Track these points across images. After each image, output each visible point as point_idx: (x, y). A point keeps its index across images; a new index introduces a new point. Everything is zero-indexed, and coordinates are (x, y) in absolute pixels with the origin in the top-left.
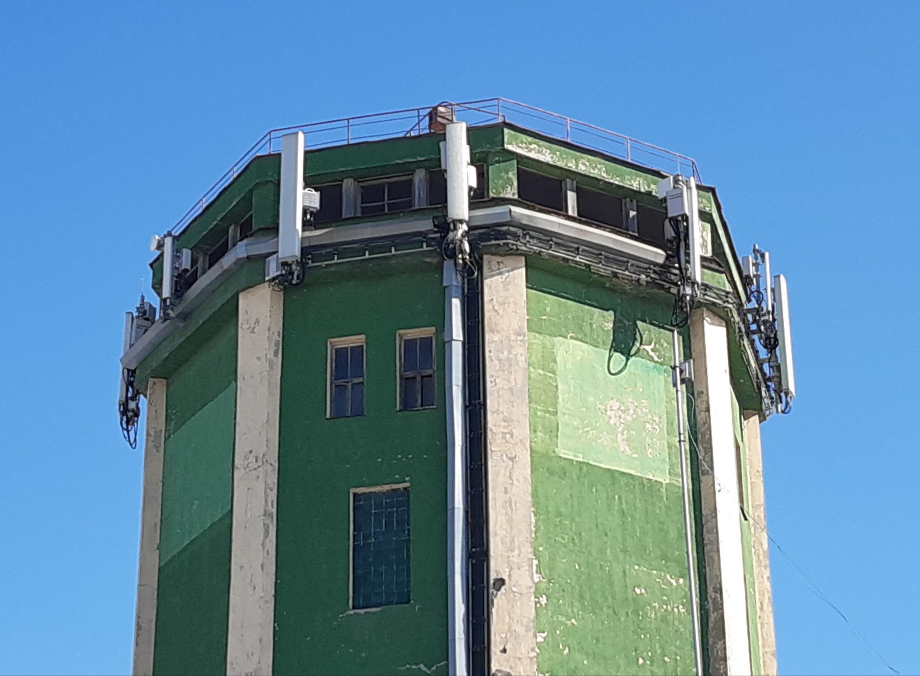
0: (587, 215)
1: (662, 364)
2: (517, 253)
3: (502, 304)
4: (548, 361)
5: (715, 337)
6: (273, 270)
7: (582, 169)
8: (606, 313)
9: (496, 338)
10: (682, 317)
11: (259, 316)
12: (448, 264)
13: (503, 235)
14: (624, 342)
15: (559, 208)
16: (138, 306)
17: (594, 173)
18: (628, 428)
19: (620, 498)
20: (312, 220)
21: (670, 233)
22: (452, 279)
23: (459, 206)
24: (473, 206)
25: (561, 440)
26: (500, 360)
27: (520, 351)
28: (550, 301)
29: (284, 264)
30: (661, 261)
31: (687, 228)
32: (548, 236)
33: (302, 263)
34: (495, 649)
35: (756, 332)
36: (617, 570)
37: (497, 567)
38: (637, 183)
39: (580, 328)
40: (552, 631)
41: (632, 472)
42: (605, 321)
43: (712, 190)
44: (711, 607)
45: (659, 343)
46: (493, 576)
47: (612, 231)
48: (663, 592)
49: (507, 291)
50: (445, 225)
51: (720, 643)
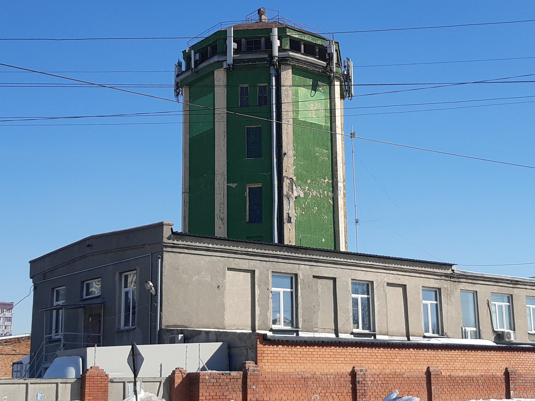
0: (306, 53)
2: (290, 65)
4: (296, 94)
5: (337, 83)
6: (225, 66)
11: (220, 77)
12: (272, 67)
13: (287, 60)
14: (314, 88)
17: (308, 40)
20: (236, 51)
21: (327, 57)
22: (273, 71)
23: (276, 53)
24: (279, 51)
25: (299, 115)
27: (290, 92)
29: (229, 65)
31: (332, 56)
32: (298, 60)
33: (233, 65)
34: (284, 171)
35: (346, 79)
36: (312, 149)
37: (284, 150)
38: (319, 42)
40: (297, 166)
42: (310, 82)
43: (338, 43)
44: (334, 157)
45: (323, 88)
46: (283, 152)
49: (287, 76)
50: (271, 57)
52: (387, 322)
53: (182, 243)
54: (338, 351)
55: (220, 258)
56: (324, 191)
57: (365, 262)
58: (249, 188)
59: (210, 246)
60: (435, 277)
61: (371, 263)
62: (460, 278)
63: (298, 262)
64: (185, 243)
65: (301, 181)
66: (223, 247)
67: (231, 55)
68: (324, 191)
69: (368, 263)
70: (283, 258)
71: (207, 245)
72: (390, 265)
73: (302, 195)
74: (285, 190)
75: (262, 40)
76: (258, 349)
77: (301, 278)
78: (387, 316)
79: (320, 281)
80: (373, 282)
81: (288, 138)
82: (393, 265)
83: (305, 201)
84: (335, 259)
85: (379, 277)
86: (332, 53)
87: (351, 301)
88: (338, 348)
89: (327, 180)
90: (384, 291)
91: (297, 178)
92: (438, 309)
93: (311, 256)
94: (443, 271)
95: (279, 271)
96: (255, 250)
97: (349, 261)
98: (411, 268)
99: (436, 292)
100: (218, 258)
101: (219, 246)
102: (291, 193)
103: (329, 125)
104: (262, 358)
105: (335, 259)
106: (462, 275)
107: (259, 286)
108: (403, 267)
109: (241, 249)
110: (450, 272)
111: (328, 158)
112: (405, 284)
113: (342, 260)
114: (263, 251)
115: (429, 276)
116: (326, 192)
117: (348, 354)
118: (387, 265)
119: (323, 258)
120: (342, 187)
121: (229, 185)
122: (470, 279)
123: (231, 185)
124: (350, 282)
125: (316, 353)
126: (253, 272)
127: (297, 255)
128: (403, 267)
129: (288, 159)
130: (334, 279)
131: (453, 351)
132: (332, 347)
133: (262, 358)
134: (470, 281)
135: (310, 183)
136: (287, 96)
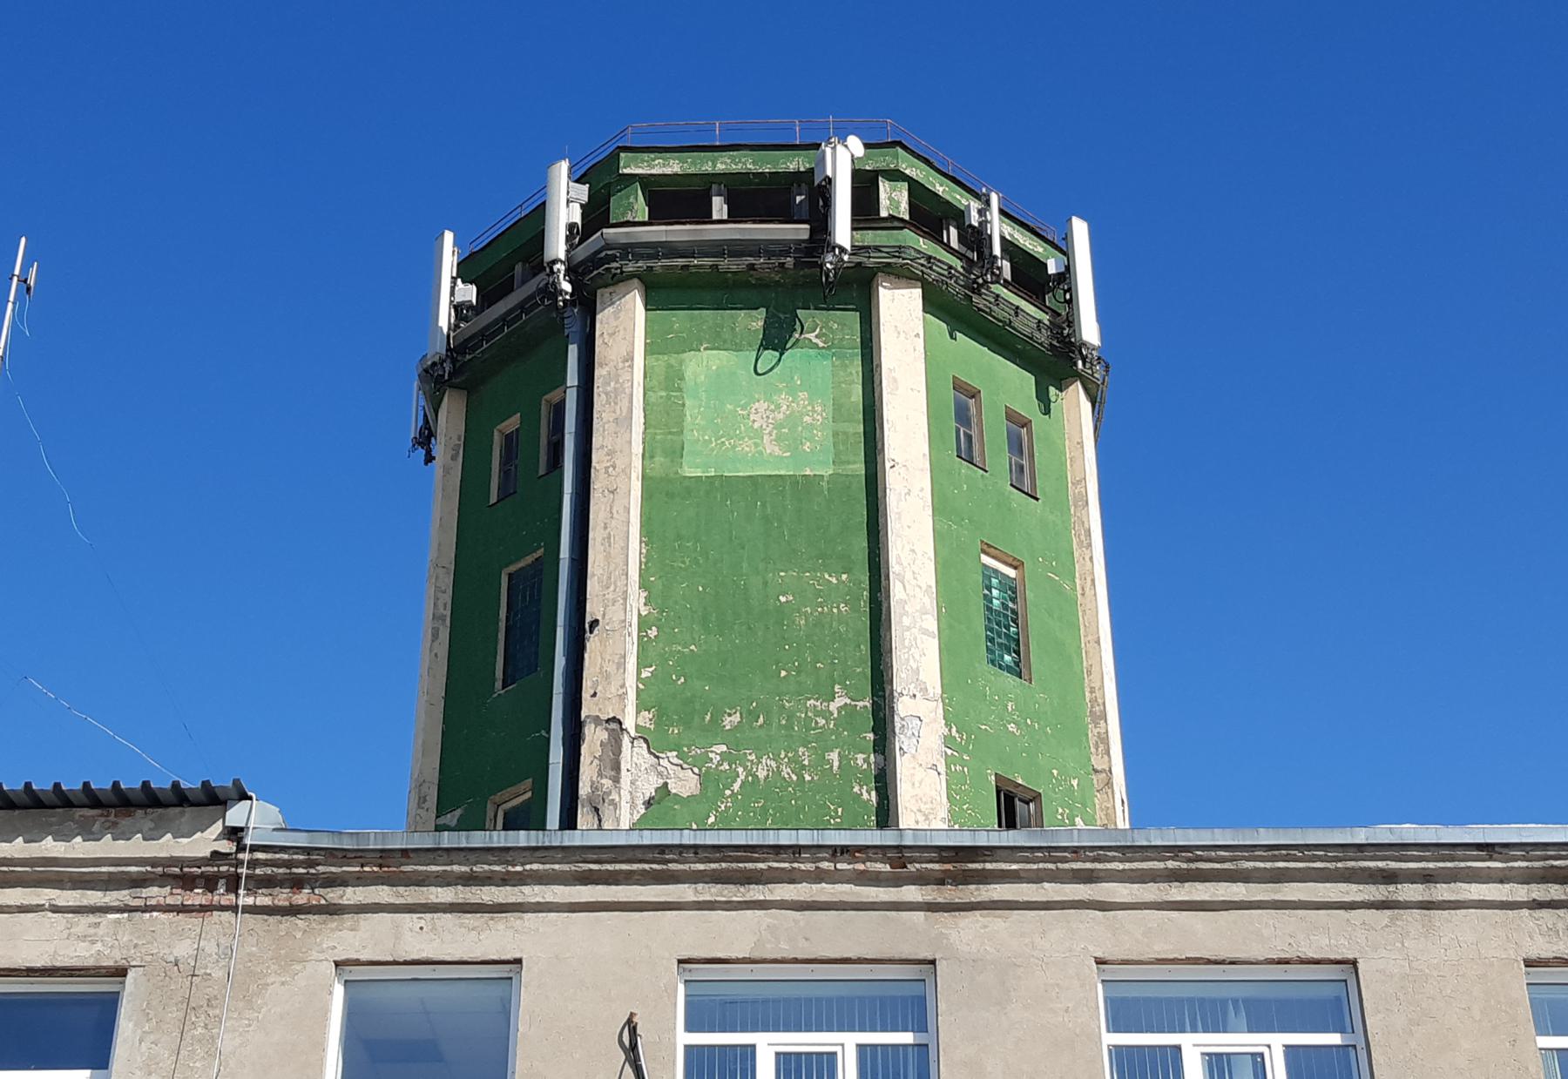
1: (829, 348)
2: (631, 276)
3: (611, 335)
7: (720, 167)
8: (754, 312)
9: (604, 372)
10: (855, 290)
14: (777, 338)
15: (704, 216)
16: (184, 785)
17: (736, 168)
18: (778, 426)
19: (763, 505)
26: (607, 394)
28: (679, 320)
30: (806, 236)
34: (586, 695)
39: (718, 334)
41: (782, 473)
42: (755, 321)
45: (824, 328)
46: (588, 619)
47: (754, 222)
48: (818, 594)
51: (627, 436)
62: (332, 882)
65: (686, 723)
94: (136, 847)
102: (607, 783)
103: (859, 468)
110: (204, 842)
111: (852, 603)
135: (736, 728)
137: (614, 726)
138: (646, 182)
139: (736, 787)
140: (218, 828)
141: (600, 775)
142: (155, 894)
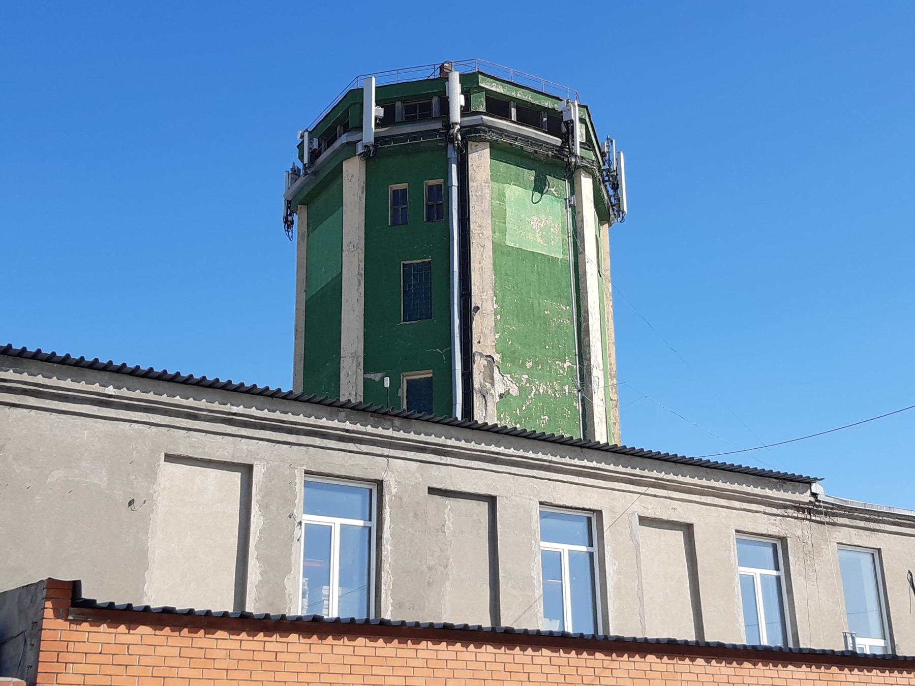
0: (521, 121)
2: (485, 140)
5: (587, 184)
6: (360, 149)
7: (519, 96)
9: (475, 184)
10: (569, 173)
11: (354, 173)
12: (450, 146)
13: (478, 131)
14: (540, 187)
15: (507, 117)
17: (525, 98)
18: (541, 230)
20: (380, 123)
21: (564, 129)
22: (452, 154)
23: (456, 116)
25: (508, 237)
29: (366, 146)
33: (375, 146)
34: (475, 342)
35: (608, 180)
36: (536, 302)
37: (475, 301)
38: (547, 103)
40: (503, 333)
42: (530, 176)
43: (586, 107)
45: (558, 186)
46: (473, 305)
49: (480, 160)
50: (448, 126)
52: (642, 616)
53: (17, 377)
54: (380, 652)
55: (145, 427)
56: (562, 385)
57: (576, 462)
58: (408, 381)
59: (110, 390)
60: (769, 510)
61: (594, 464)
63: (385, 451)
64: (25, 377)
65: (513, 362)
66: (151, 396)
67: (370, 131)
68: (562, 385)
69: (585, 463)
70: (341, 439)
71: (101, 390)
72: (646, 473)
73: (514, 391)
74: (478, 380)
75: (433, 101)
76: (45, 635)
77: (394, 491)
78: (641, 600)
79: (450, 502)
80: (601, 512)
81: (482, 277)
82: (655, 474)
83: (521, 402)
84: (493, 448)
85: (620, 503)
86: (572, 121)
87: (539, 558)
88: (381, 642)
89: (568, 364)
90: (632, 537)
91: (503, 358)
92: (783, 589)
93: (422, 437)
94: (789, 496)
95: (327, 471)
96: (253, 411)
97: (531, 454)
98: (704, 482)
99: (775, 547)
100: (135, 426)
101: (137, 394)
102: (488, 385)
104: (57, 667)
105: (493, 448)
106: (840, 507)
107: (264, 507)
108: (680, 478)
109: (210, 406)
110: (806, 497)
112: (688, 521)
113: (511, 451)
114: (278, 415)
115: (754, 507)
116: (566, 388)
117: (422, 663)
118: (637, 471)
119: (458, 444)
120: (602, 378)
121: (368, 376)
122: (862, 519)
123: (371, 376)
124: (536, 510)
125: (294, 657)
126: (247, 470)
127: (380, 431)
128: (680, 478)
129: (482, 318)
130: (492, 501)
131: (790, 667)
132: (361, 641)
133: (57, 667)
134: (862, 524)
135: (532, 368)
136: (481, 199)
137: (489, 359)
138: (487, 91)
139: (532, 395)
140: (809, 493)
141: (484, 380)
142: (790, 512)
